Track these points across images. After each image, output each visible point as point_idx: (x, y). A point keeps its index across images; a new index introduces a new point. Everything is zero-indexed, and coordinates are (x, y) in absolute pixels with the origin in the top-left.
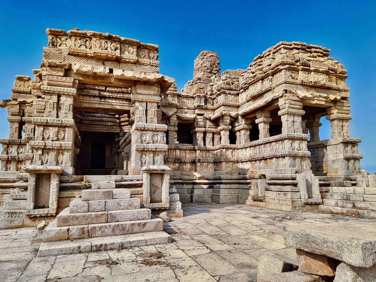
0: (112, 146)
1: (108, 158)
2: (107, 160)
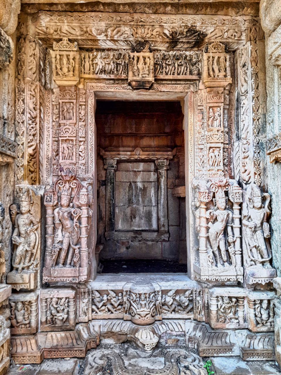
0: (232, 108)
1: (211, 204)
2: (203, 213)
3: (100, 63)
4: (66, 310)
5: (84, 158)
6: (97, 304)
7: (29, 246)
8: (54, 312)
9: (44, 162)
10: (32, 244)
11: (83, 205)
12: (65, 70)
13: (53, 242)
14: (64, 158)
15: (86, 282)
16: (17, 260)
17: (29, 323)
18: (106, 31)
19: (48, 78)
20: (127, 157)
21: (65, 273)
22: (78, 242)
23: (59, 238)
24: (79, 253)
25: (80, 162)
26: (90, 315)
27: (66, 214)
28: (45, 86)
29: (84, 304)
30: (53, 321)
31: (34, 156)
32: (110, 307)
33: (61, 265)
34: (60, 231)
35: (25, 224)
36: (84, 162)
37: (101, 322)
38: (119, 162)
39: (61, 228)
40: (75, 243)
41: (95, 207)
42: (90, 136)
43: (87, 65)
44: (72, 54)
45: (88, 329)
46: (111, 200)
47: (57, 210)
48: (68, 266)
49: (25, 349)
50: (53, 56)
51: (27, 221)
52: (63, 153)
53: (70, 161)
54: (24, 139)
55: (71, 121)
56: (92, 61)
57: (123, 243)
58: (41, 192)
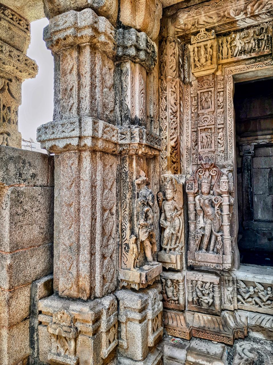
3: (239, 44)
4: (211, 295)
5: (224, 148)
6: (243, 294)
7: (174, 230)
8: (199, 294)
9: (184, 152)
10: (177, 228)
11: (224, 193)
12: (203, 60)
13: (196, 227)
14: (203, 147)
15: (229, 271)
16: (165, 242)
17: (178, 300)
18: (246, 8)
19: (186, 73)
20: (267, 141)
21: (208, 258)
22: (220, 230)
23: (201, 224)
24: (222, 240)
25: (219, 149)
26: (236, 305)
27: (207, 201)
28: (184, 81)
29: (229, 291)
30: (199, 303)
31: (176, 148)
32: (258, 300)
33: (204, 250)
34: (201, 217)
35: (170, 210)
36: (223, 149)
37: (248, 314)
38: (257, 147)
39: (202, 214)
40: (217, 230)
41: (235, 194)
42: (228, 122)
43: (225, 50)
44: (209, 43)
45: (235, 318)
46: (249, 188)
47: (198, 197)
48: (211, 252)
49: (175, 323)
50: (191, 50)
51: (172, 207)
52: (202, 142)
53: (209, 149)
54: (167, 133)
55: (209, 110)
56: (230, 44)
57: (264, 234)
58: (183, 181)
